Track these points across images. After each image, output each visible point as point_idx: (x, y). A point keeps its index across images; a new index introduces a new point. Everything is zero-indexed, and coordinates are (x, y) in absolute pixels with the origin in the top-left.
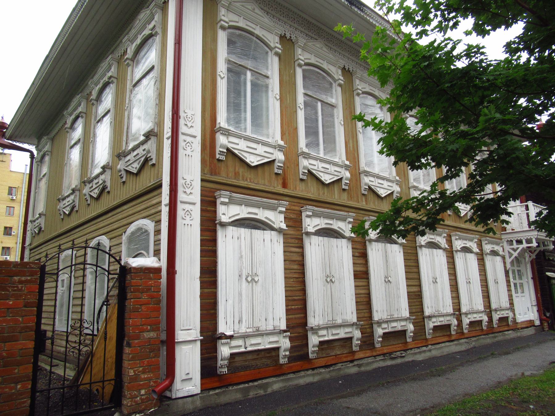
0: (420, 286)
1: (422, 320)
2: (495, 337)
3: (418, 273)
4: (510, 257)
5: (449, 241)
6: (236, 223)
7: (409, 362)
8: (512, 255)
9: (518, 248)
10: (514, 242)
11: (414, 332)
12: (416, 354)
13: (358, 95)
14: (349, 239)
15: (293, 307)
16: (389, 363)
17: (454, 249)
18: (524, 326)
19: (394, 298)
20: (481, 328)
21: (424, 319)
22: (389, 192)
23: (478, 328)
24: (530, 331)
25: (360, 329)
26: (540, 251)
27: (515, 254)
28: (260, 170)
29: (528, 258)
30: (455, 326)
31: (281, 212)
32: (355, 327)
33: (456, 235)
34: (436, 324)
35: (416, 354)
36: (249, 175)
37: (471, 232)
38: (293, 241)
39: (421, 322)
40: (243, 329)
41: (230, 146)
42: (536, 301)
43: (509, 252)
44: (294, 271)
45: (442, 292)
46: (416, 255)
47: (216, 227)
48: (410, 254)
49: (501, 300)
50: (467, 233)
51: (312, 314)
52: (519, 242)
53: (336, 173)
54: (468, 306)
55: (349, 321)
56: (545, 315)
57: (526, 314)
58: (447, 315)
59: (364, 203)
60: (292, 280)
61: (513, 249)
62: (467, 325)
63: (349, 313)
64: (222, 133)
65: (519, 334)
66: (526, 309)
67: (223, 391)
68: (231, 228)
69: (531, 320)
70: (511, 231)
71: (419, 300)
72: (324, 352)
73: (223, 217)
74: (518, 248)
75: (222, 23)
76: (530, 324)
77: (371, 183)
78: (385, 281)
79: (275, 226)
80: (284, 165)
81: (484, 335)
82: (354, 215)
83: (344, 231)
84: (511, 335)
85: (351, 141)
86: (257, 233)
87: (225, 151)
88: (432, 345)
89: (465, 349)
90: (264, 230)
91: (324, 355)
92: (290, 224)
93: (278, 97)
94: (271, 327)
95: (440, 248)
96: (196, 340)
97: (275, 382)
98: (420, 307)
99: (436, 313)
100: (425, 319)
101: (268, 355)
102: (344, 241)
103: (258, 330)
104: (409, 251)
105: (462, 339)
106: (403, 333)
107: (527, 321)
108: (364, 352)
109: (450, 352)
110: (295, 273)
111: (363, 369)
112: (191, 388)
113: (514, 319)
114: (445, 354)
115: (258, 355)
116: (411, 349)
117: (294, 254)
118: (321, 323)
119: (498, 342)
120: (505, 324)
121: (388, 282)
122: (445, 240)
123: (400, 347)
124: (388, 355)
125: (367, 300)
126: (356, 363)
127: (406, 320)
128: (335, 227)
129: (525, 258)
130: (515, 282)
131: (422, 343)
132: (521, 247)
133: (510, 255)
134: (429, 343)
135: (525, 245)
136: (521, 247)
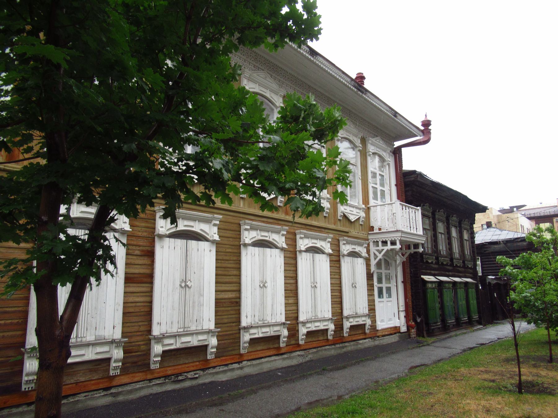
0: (239, 291)
1: (237, 331)
2: (343, 347)
3: (239, 276)
4: (375, 259)
5: (292, 240)
7: (204, 384)
8: (377, 257)
9: (383, 250)
10: (380, 243)
11: (218, 347)
12: (217, 373)
13: (370, 155)
14: (282, 249)
16: (170, 387)
17: (298, 249)
18: (387, 333)
19: (194, 306)
20: (325, 338)
21: (240, 330)
22: (358, 217)
23: (321, 338)
24: (394, 338)
25: (217, 336)
26: (411, 253)
27: (380, 256)
29: (399, 259)
30: (332, 331)
31: (215, 225)
32: (330, 321)
33: (301, 233)
34: (352, 324)
35: (217, 373)
37: (327, 231)
39: (236, 333)
40: (175, 329)
42: (404, 307)
43: (375, 254)
45: (273, 299)
46: (239, 255)
48: (228, 254)
49: (358, 306)
50: (321, 232)
52: (385, 243)
54: (310, 313)
55: (106, 337)
56: (415, 320)
57: (390, 320)
61: (378, 250)
62: (303, 335)
63: (109, 327)
65: (377, 343)
66: (391, 314)
69: (396, 327)
70: (378, 231)
71: (236, 308)
73: (161, 229)
74: (383, 250)
76: (395, 330)
77: (345, 211)
78: (181, 286)
79: (208, 237)
81: (329, 345)
83: (208, 234)
84: (367, 343)
88: (248, 360)
89: (297, 363)
92: (289, 243)
95: (323, 253)
98: (237, 316)
99: (260, 323)
100: (241, 331)
102: (324, 256)
103: (356, 314)
104: (228, 250)
105: (297, 351)
106: (203, 348)
107: (391, 328)
108: (131, 375)
109: (273, 368)
111: (121, 398)
113: (373, 327)
114: (265, 370)
116: (214, 367)
118: (169, 331)
119: (346, 353)
120: (360, 332)
121: (185, 286)
122: (329, 244)
123: (196, 366)
124: (175, 377)
125: (146, 309)
126: (113, 391)
127: (209, 332)
128: (318, 245)
129: (396, 261)
130: (380, 285)
131: (233, 359)
132: (386, 248)
133: (376, 257)
134: (245, 358)
135: (389, 247)
136: (386, 248)
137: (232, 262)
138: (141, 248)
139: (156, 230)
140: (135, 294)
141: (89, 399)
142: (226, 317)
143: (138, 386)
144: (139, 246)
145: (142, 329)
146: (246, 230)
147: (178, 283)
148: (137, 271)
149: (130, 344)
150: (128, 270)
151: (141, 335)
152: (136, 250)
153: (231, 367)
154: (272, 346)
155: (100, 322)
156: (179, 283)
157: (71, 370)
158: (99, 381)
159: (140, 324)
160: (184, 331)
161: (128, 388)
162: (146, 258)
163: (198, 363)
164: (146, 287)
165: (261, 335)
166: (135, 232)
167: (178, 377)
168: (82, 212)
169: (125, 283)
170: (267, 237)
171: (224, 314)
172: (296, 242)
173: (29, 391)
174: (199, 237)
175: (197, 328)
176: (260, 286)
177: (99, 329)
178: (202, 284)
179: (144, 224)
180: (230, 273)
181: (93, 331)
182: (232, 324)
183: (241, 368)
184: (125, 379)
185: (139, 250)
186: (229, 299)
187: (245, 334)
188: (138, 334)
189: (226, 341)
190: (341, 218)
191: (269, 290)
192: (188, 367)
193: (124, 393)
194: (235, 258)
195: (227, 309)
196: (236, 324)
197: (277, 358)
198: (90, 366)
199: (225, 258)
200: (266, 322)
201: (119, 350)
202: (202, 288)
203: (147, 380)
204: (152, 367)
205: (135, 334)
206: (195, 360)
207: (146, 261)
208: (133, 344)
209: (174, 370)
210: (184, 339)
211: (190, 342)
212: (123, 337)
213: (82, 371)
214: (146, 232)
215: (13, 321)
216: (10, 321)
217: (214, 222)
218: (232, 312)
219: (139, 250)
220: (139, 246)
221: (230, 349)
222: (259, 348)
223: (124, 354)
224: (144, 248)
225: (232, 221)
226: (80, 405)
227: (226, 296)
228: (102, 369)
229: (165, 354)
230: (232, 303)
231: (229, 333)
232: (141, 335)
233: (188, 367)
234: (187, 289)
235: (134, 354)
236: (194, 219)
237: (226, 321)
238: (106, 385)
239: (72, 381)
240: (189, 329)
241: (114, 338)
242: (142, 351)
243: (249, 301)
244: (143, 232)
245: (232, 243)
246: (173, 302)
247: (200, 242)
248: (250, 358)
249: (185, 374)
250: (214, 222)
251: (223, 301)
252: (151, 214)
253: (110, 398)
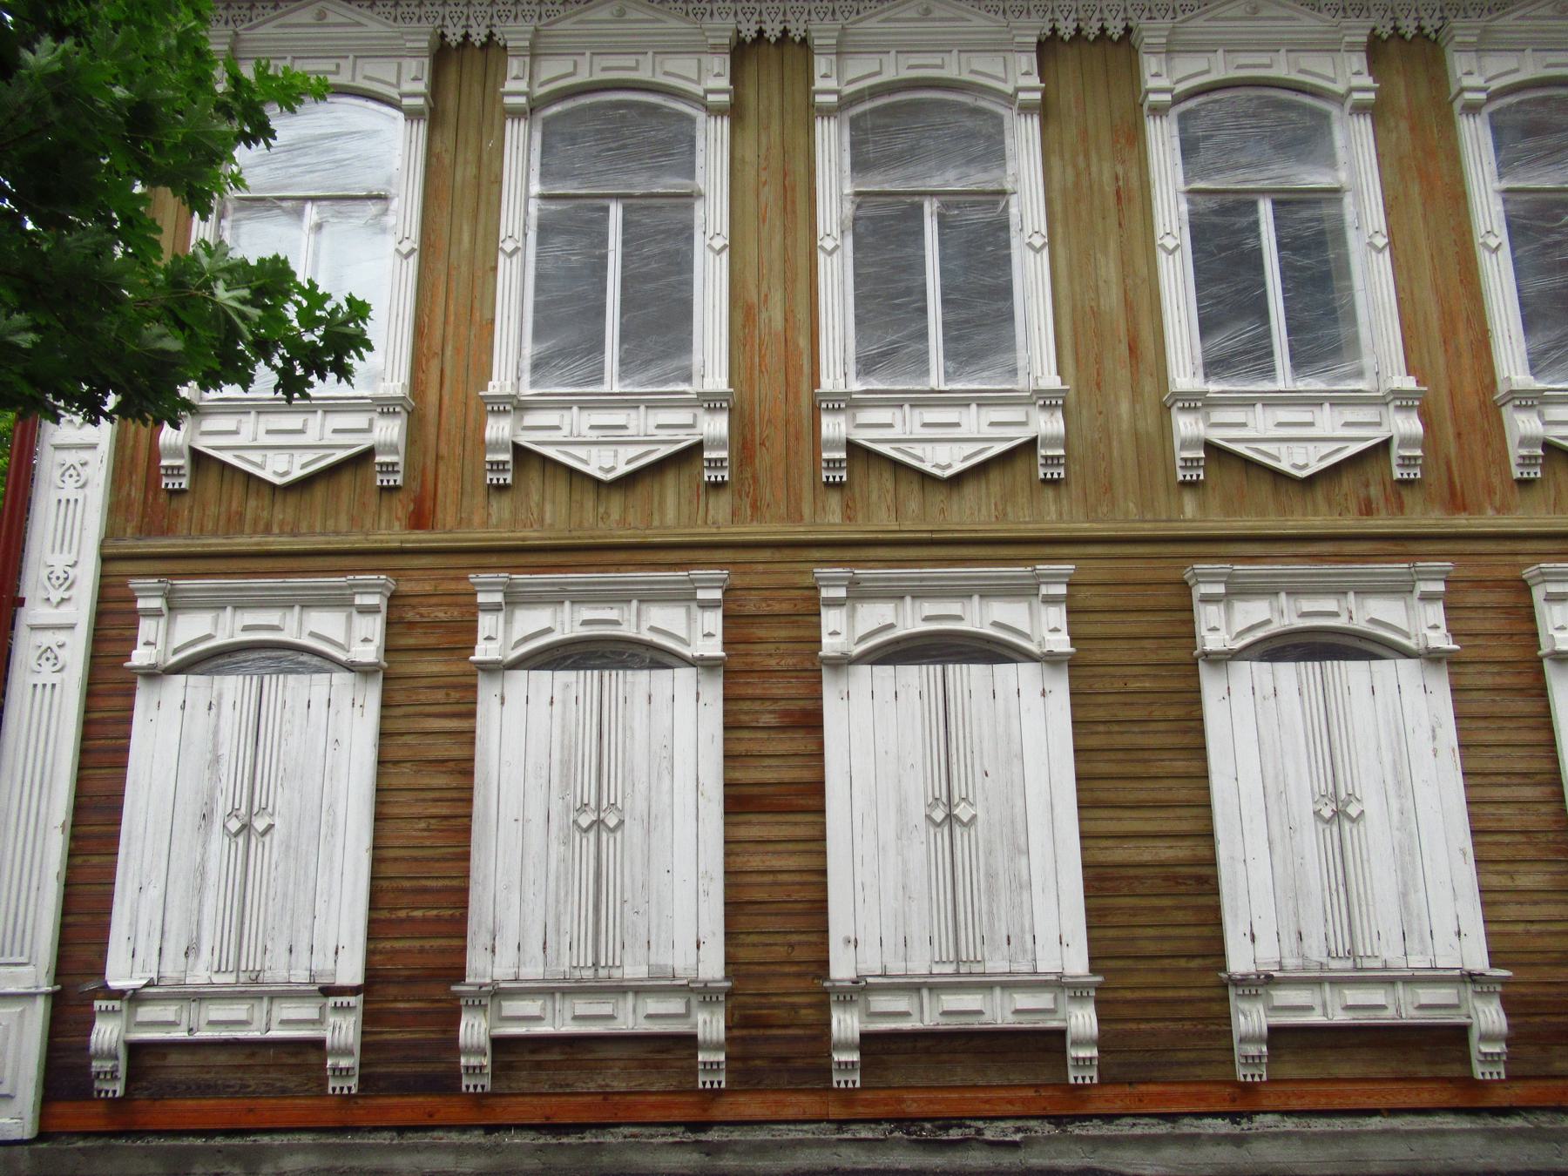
0: (1209, 835)
6: (539, 659)
15: (418, 913)
25: (1098, 1003)
28: (319, 492)
36: (284, 512)
38: (440, 695)
41: (1216, 436)
44: (437, 795)
47: (1196, 675)
53: (663, 435)
58: (1059, 984)
60: (422, 825)
63: (1445, 929)
64: (1183, 409)
67: (102, 1148)
68: (1243, 668)
72: (543, 1075)
75: (1468, 96)
80: (1066, 448)
85: (777, 297)
87: (1540, 452)
90: (1016, 662)
91: (546, 1088)
93: (1381, 241)
94: (301, 976)
96: (33, 996)
97: (291, 1150)
99: (1335, 964)
101: (292, 1061)
103: (255, 981)
104: (1134, 685)
108: (772, 1097)
110: (435, 800)
111: (728, 1162)
112: (7, 1121)
115: (253, 1055)
116: (1109, 1118)
117: (441, 740)
118: (896, 967)
126: (713, 1136)
127: (700, 993)
131: (1201, 1097)
137: (1161, 726)
138: (782, 705)
139: (1542, 639)
140: (770, 847)
141: (632, 1146)
142: (1151, 932)
143: (795, 1133)
144: (775, 700)
146: (1208, 599)
147: (918, 811)
150: (1086, 767)
151: (798, 975)
152: (762, 712)
153: (1187, 1127)
154: (1423, 1071)
155: (659, 926)
156: (922, 812)
157: (589, 1056)
158: (670, 1098)
159: (795, 938)
160: (958, 974)
161: (761, 1135)
162: (799, 734)
163: (1031, 1093)
164: (806, 824)
165: (1340, 1018)
166: (758, 659)
167: (946, 1128)
170: (1336, 614)
172: (1532, 618)
174: (1006, 652)
175: (1015, 968)
176: (1317, 813)
177: (658, 946)
178: (1019, 809)
179: (783, 633)
180: (1153, 771)
181: (641, 952)
182: (1183, 963)
183: (1238, 1141)
184: (752, 1107)
186: (1162, 865)
187: (1245, 1005)
188: (787, 969)
189: (1160, 1025)
190: (1536, 473)
191: (1376, 834)
192: (987, 1101)
193: (738, 1149)
194: (1173, 713)
195: (1156, 902)
196: (1209, 962)
197: (1465, 1123)
198: (638, 1052)
199: (1123, 714)
200: (1367, 963)
201: (712, 1013)
202: (1020, 826)
203: (829, 1121)
205: (778, 968)
206: (1016, 1078)
207: (798, 742)
208: (774, 999)
209: (931, 1102)
210: (952, 1002)
213: (621, 1064)
214: (793, 654)
216: (435, 912)
217: (1423, 587)
218: (1180, 916)
219: (771, 712)
220: (775, 700)
222: (1344, 1070)
223: (1099, 1021)
224: (792, 706)
226: (606, 1160)
227: (1147, 857)
228: (679, 1064)
229: (868, 1040)
230: (1176, 880)
231: (1170, 994)
232: (798, 975)
233: (987, 1101)
234: (1347, 825)
236: (962, 593)
237: (1151, 948)
238: (693, 1114)
240: (977, 968)
241: (702, 976)
242: (804, 1026)
243: (1261, 873)
244: (782, 656)
246: (905, 873)
248: (1295, 1104)
249: (980, 1124)
250: (1423, 587)
251: (1131, 872)
252: (805, 599)
253: (695, 1156)
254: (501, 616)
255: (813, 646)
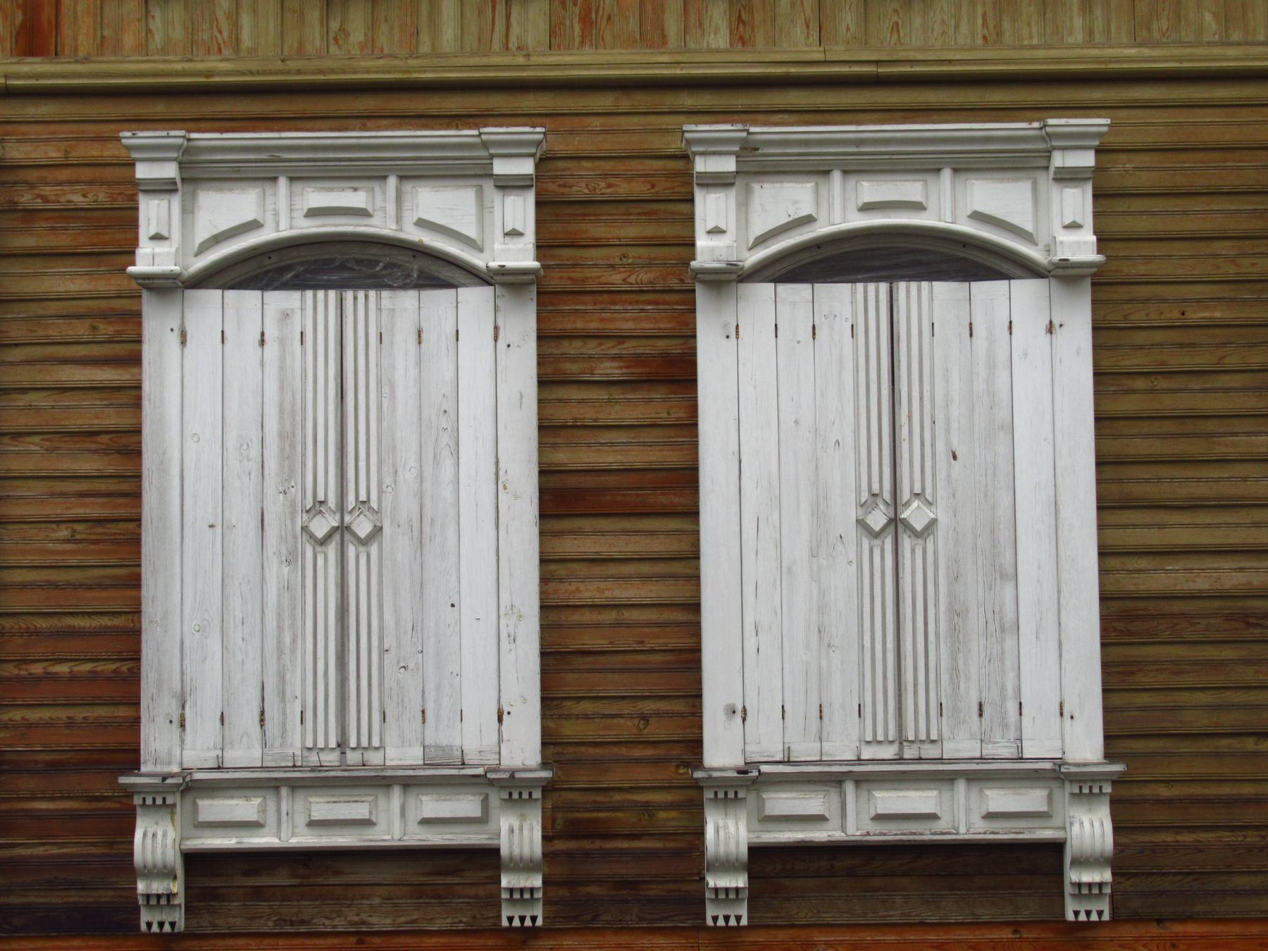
25: (1115, 803)
31: (1068, 177)
38: (81, 329)
40: (842, 746)
44: (84, 486)
51: (168, 706)
55: (471, 757)
59: (720, 39)
60: (64, 533)
72: (264, 907)
82: (534, 133)
86: (369, 307)
117: (86, 400)
118: (805, 749)
138: (629, 347)
140: (612, 569)
142: (1203, 698)
144: (621, 338)
145: (658, 730)
147: (844, 512)
148: (611, 459)
149: (600, 798)
155: (439, 688)
159: (649, 707)
160: (900, 759)
164: (668, 533)
168: (313, 213)
169: (543, 516)
171: (1186, 680)
173: (1089, 925)
175: (989, 750)
178: (1003, 513)
179: (632, 231)
180: (1221, 448)
185: (618, 358)
188: (637, 752)
189: (1210, 836)
201: (523, 817)
202: (1004, 536)
204: (713, 913)
205: (624, 751)
208: (618, 797)
211: (933, 817)
212: (1109, 756)
213: (383, 891)
214: (649, 265)
215: (101, 667)
216: (88, 667)
219: (618, 358)
220: (621, 338)
221: (1242, 881)
224: (645, 348)
225: (1229, 136)
227: (1202, 583)
228: (471, 891)
229: (761, 858)
231: (1227, 790)
232: (655, 762)
235: (624, 844)
236: (924, 164)
237: (1202, 722)
239: (340, 924)
240: (930, 751)
244: (632, 267)
245: (1230, 270)
246: (822, 609)
247: (982, 289)
251: (1176, 607)
252: (670, 175)
254: (176, 201)
255: (683, 251)
